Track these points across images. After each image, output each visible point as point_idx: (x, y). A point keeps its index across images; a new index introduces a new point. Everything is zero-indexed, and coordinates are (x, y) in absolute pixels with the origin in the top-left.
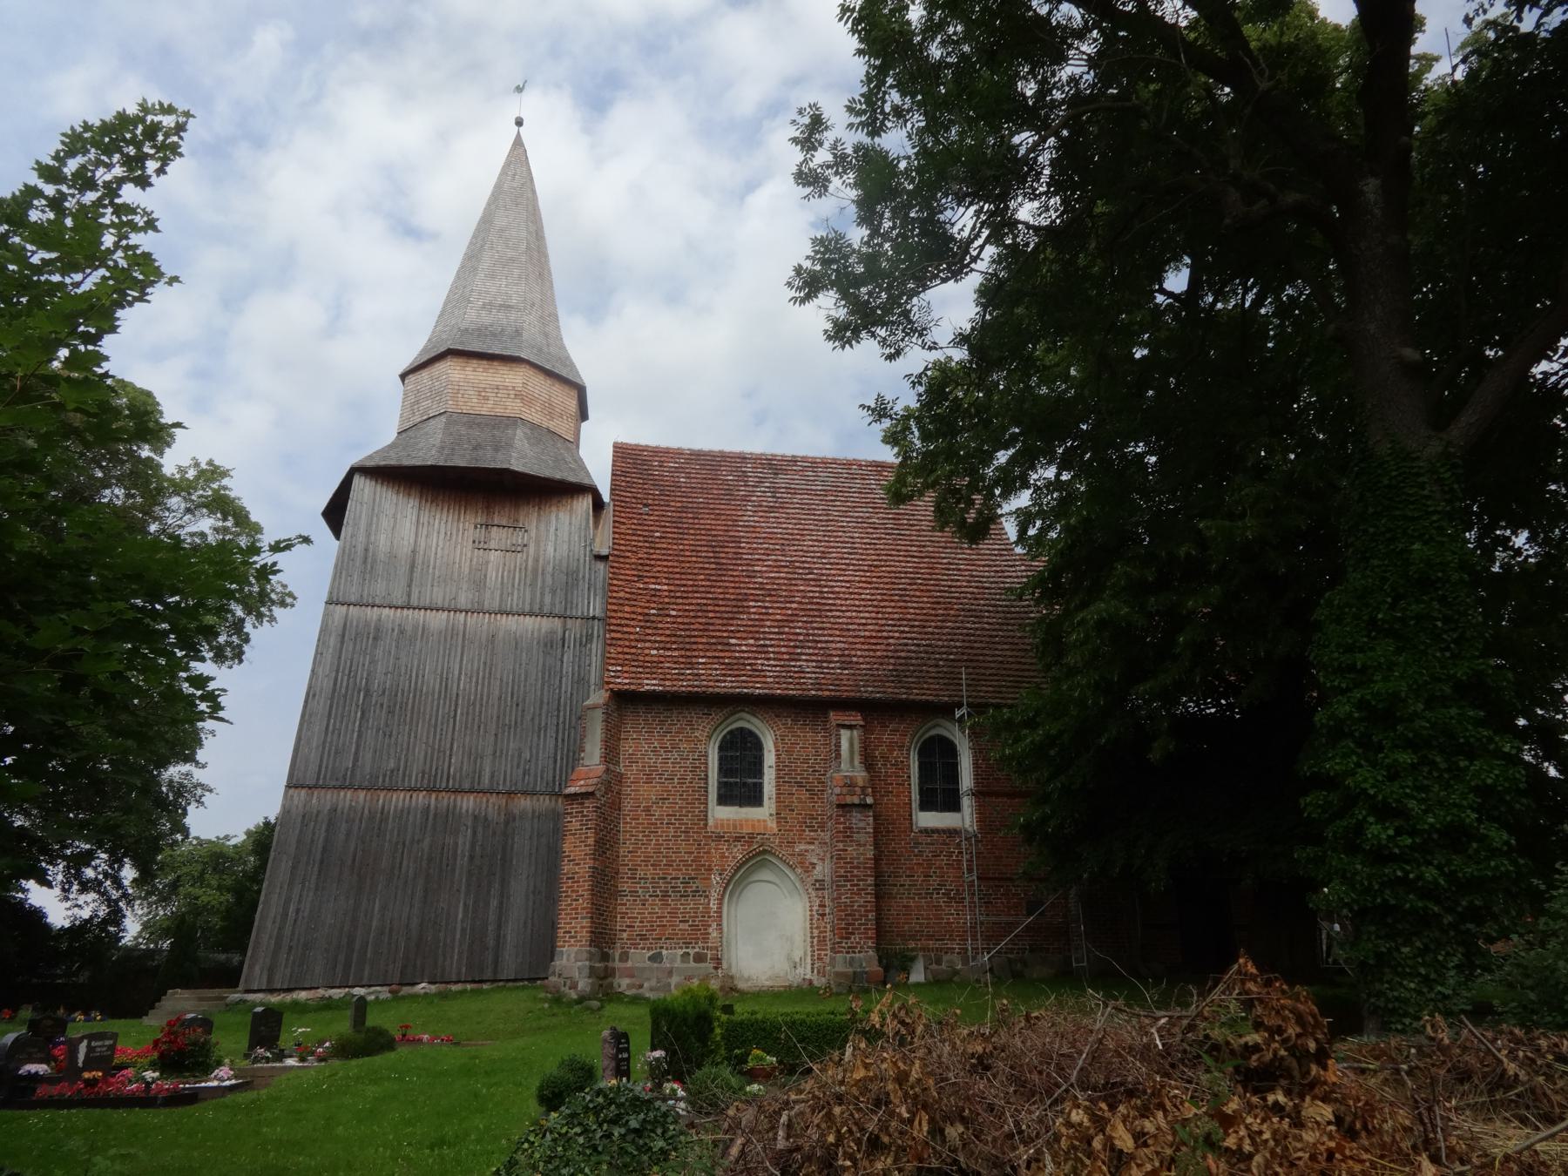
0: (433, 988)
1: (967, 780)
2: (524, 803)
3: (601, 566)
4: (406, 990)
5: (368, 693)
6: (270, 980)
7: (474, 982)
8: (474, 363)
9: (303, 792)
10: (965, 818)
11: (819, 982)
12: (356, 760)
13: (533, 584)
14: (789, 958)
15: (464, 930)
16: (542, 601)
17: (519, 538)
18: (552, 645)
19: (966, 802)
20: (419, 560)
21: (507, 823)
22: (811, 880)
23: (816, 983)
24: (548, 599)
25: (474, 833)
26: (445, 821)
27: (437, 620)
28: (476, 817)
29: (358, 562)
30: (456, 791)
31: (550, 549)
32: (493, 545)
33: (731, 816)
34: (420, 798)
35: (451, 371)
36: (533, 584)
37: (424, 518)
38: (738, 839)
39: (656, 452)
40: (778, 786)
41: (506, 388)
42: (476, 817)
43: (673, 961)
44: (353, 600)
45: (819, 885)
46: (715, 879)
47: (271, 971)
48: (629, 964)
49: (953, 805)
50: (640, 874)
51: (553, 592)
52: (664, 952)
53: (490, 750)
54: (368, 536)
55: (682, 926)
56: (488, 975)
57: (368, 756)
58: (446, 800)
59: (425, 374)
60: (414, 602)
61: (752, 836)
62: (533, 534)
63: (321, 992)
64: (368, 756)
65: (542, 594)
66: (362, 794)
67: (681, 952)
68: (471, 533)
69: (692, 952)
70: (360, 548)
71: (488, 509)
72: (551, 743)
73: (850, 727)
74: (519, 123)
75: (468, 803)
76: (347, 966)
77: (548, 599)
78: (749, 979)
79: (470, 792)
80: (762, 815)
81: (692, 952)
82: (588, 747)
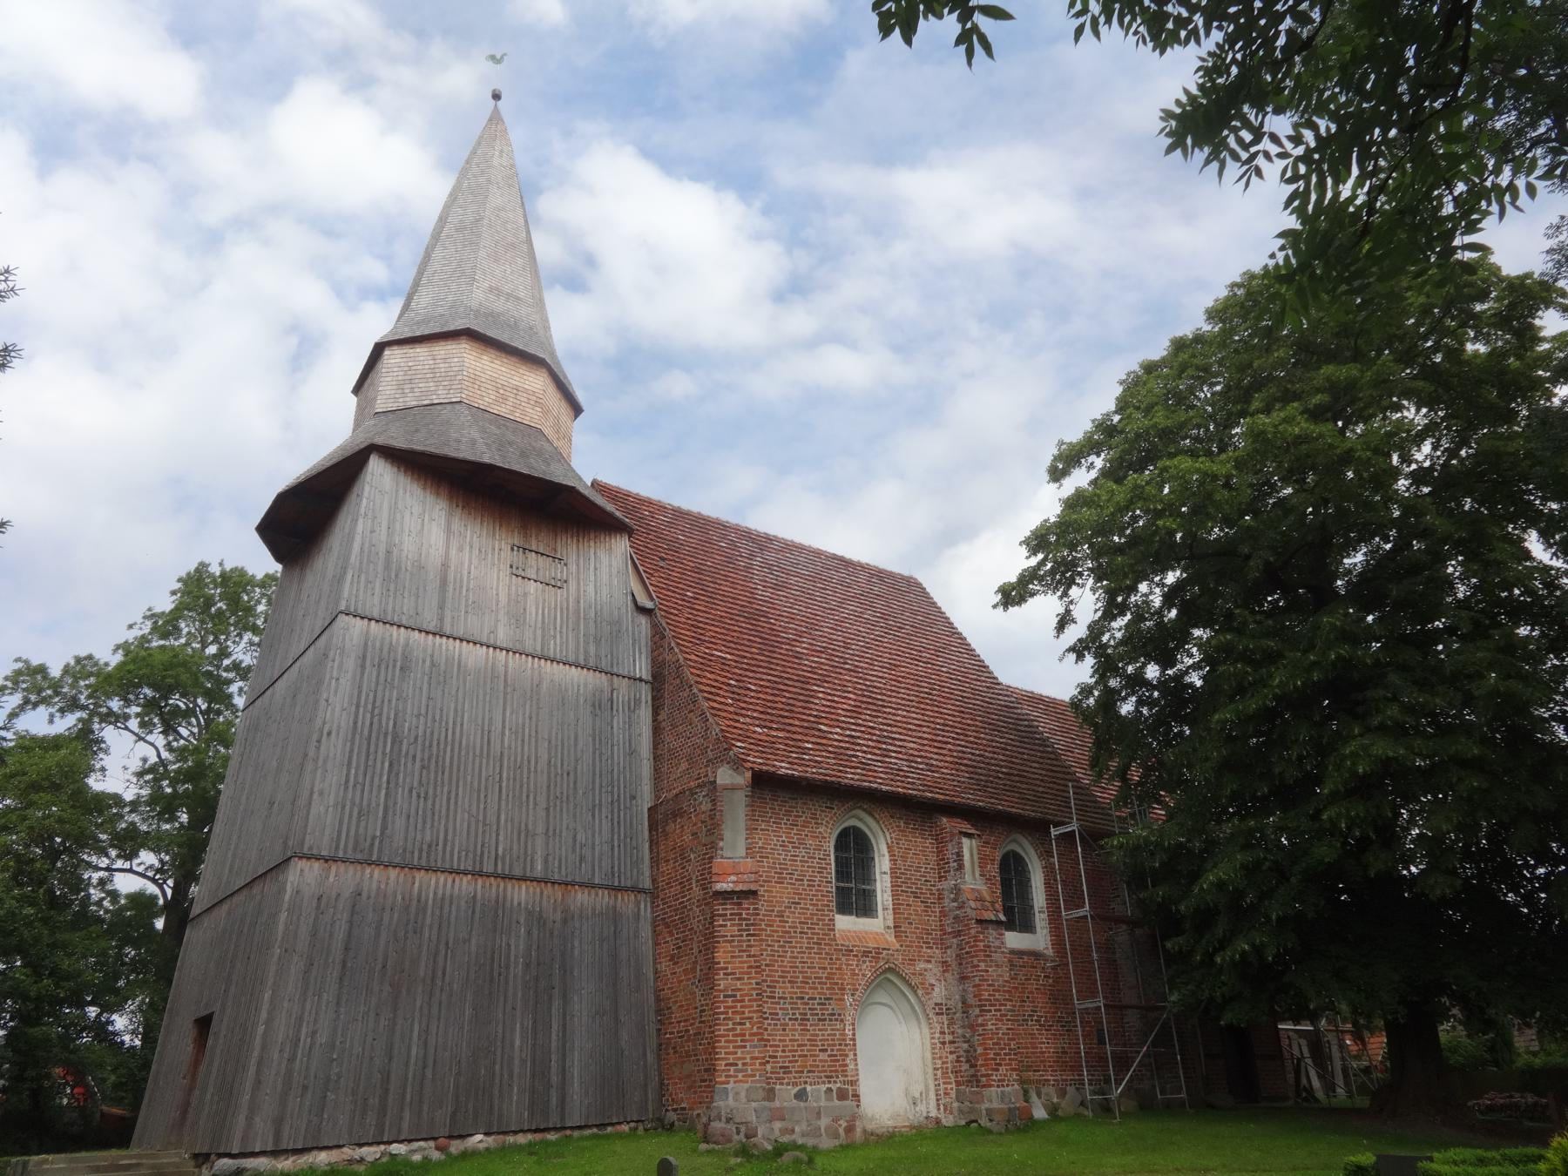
0: (490, 1139)
1: (1039, 897)
2: (581, 898)
3: (643, 621)
4: (456, 1147)
5: (397, 740)
6: (277, 1136)
7: (536, 1131)
8: (493, 353)
9: (316, 865)
10: (1039, 940)
11: (948, 1121)
12: (384, 828)
13: (576, 629)
14: (907, 1092)
15: (523, 1061)
16: (586, 652)
17: (558, 571)
18: (601, 705)
19: (1041, 920)
20: (451, 578)
21: (565, 921)
22: (931, 1003)
23: (944, 1122)
24: (592, 650)
25: (529, 933)
26: (495, 916)
27: (474, 656)
28: (530, 913)
29: (380, 568)
30: (504, 878)
31: (591, 589)
32: (531, 573)
33: (850, 927)
34: (464, 884)
35: (465, 355)
36: (576, 629)
37: (457, 525)
38: (866, 954)
39: (649, 502)
40: (895, 895)
41: (526, 391)
42: (530, 913)
43: (818, 1099)
44: (375, 615)
45: (940, 1009)
46: (848, 1000)
47: (278, 1123)
48: (777, 1104)
49: (1027, 927)
50: (779, 992)
51: (598, 641)
52: (809, 1088)
53: (540, 829)
54: (390, 534)
55: (823, 1056)
56: (554, 1120)
57: (400, 823)
58: (494, 888)
59: (421, 351)
60: (448, 630)
61: (878, 951)
62: (573, 568)
63: (347, 1152)
64: (400, 823)
65: (587, 643)
66: (393, 873)
67: (824, 1088)
68: (507, 556)
69: (834, 1087)
70: (382, 549)
71: (524, 528)
72: (606, 826)
73: (969, 836)
74: (496, 96)
75: (520, 894)
76: (382, 1110)
77: (592, 650)
78: (872, 1119)
79: (524, 879)
80: (876, 927)
81: (834, 1087)
82: (727, 834)
